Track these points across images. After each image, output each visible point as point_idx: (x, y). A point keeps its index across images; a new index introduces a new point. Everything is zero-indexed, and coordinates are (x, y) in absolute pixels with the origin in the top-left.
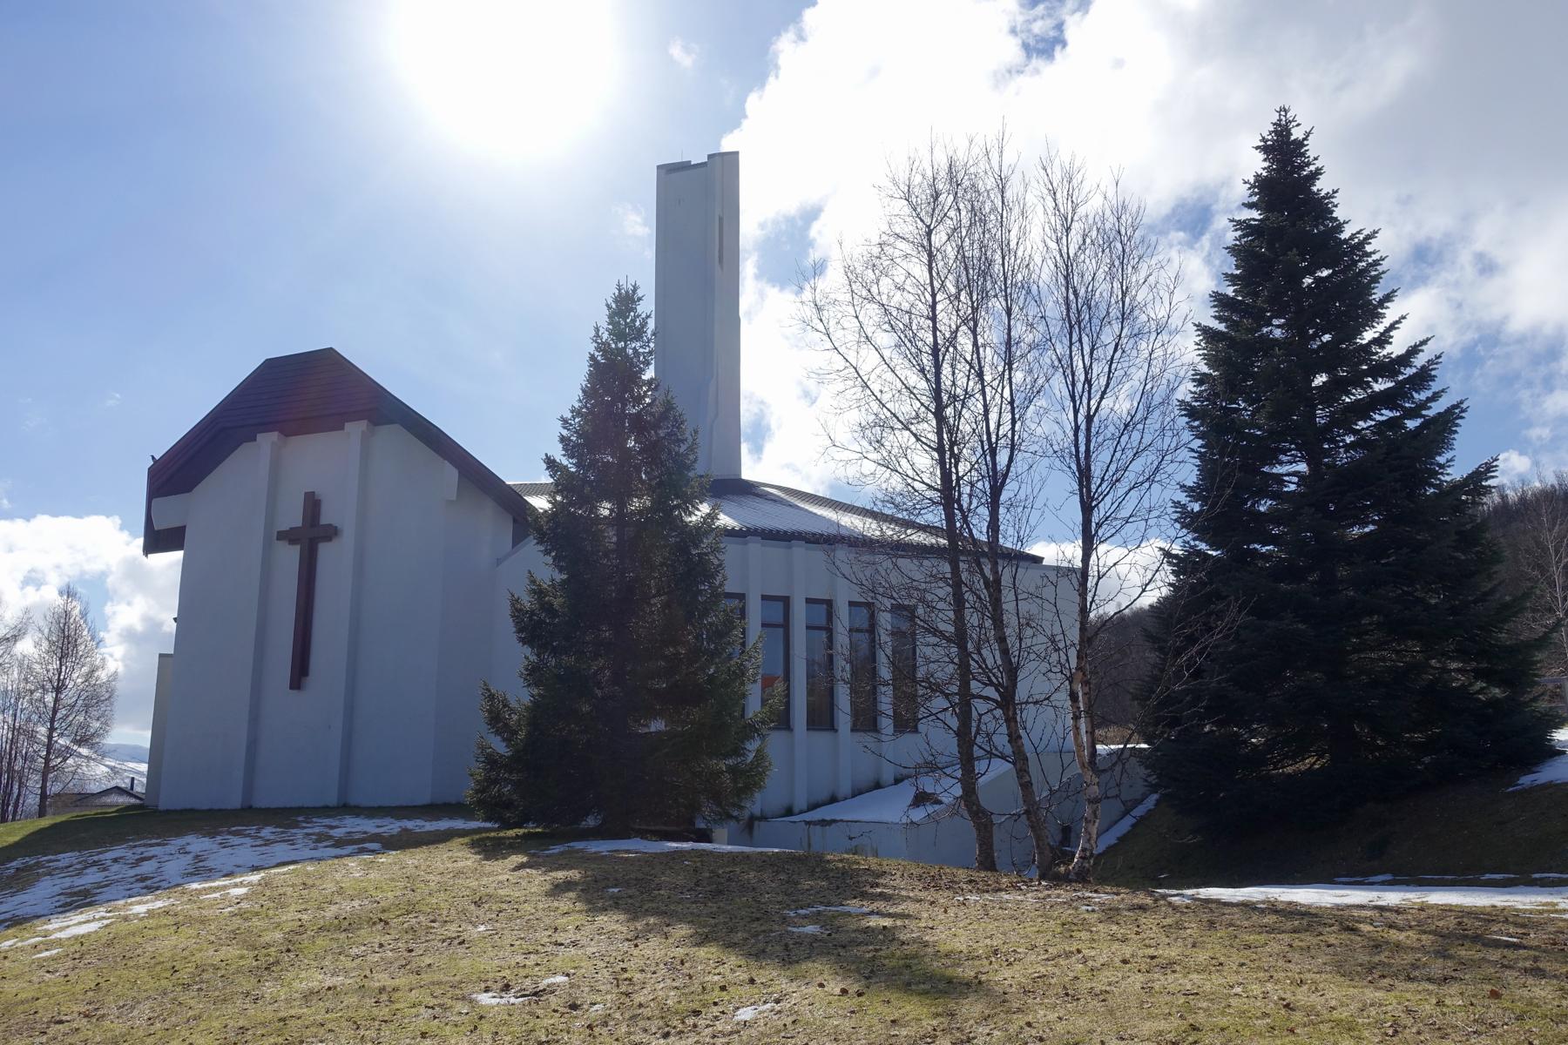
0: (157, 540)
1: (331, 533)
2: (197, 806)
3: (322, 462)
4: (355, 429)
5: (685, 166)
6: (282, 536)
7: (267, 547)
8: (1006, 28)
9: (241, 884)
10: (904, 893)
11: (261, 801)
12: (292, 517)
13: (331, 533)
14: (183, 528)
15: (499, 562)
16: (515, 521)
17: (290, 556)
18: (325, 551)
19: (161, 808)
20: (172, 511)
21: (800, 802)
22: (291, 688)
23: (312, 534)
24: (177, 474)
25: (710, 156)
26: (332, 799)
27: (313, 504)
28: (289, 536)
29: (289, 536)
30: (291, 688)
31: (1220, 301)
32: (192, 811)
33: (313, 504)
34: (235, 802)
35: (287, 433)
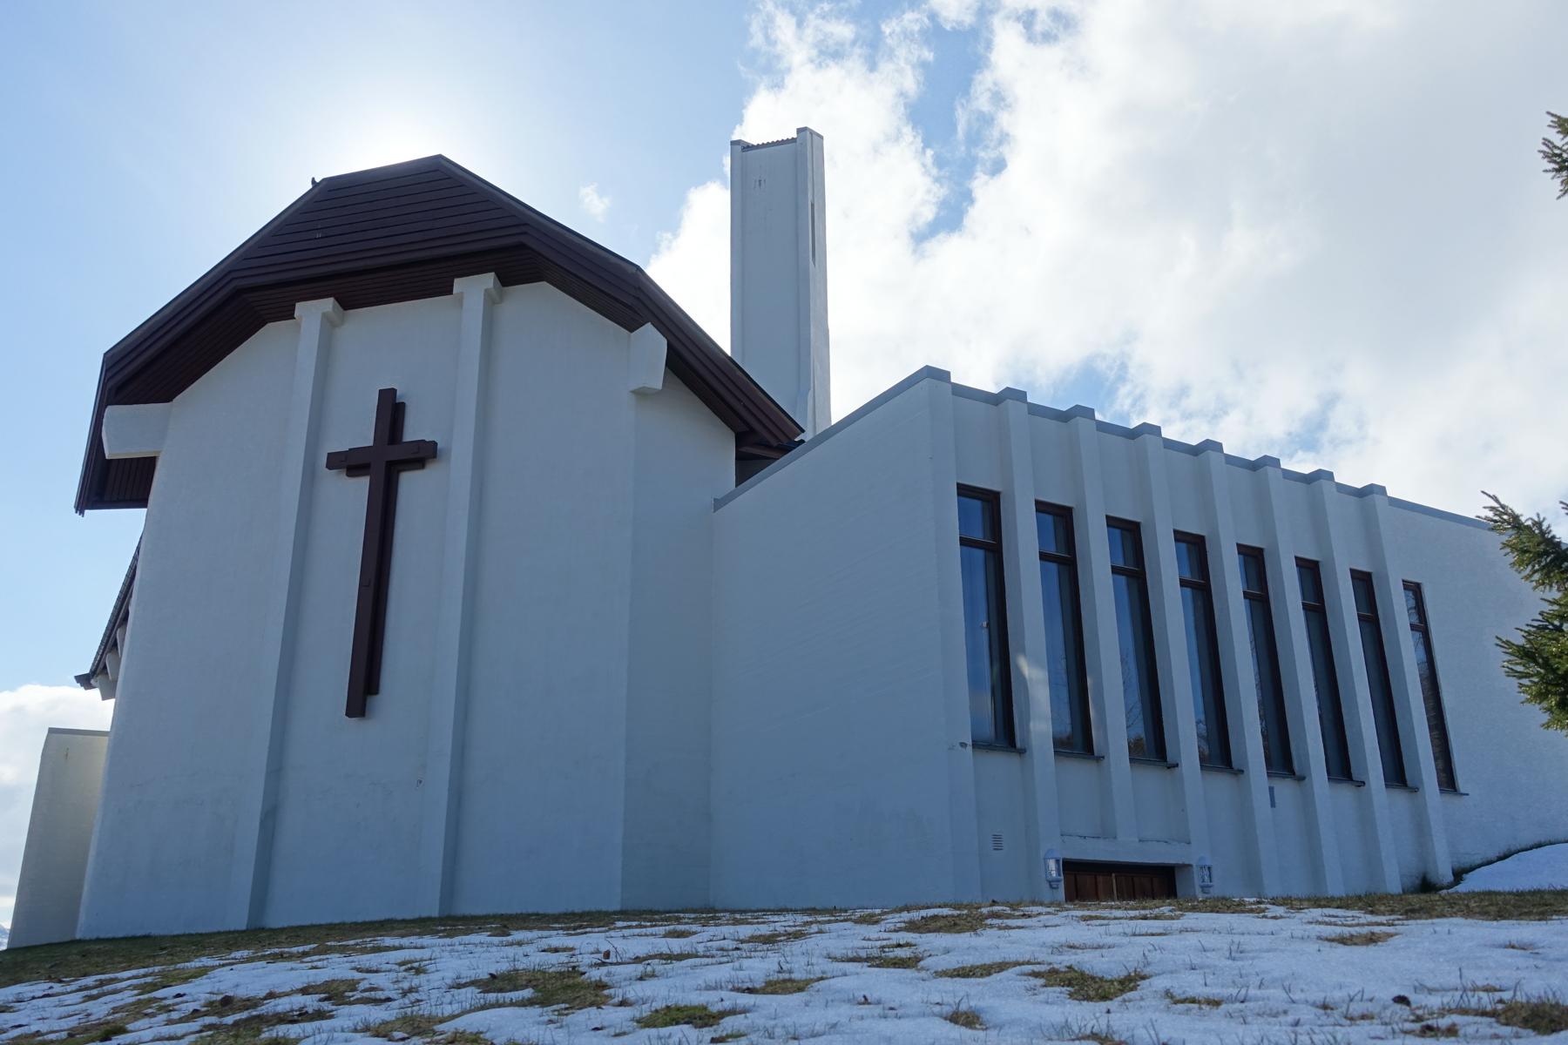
0: (111, 481)
1: (424, 455)
2: (155, 932)
3: (425, 348)
4: (474, 289)
7: (309, 479)
10: (985, 911)
12: (359, 432)
15: (719, 504)
18: (409, 482)
20: (133, 430)
21: (1444, 873)
22: (349, 713)
23: (389, 456)
24: (158, 363)
27: (391, 410)
28: (349, 463)
29: (349, 463)
30: (349, 713)
31: (937, 180)
33: (391, 410)
35: (507, 279)
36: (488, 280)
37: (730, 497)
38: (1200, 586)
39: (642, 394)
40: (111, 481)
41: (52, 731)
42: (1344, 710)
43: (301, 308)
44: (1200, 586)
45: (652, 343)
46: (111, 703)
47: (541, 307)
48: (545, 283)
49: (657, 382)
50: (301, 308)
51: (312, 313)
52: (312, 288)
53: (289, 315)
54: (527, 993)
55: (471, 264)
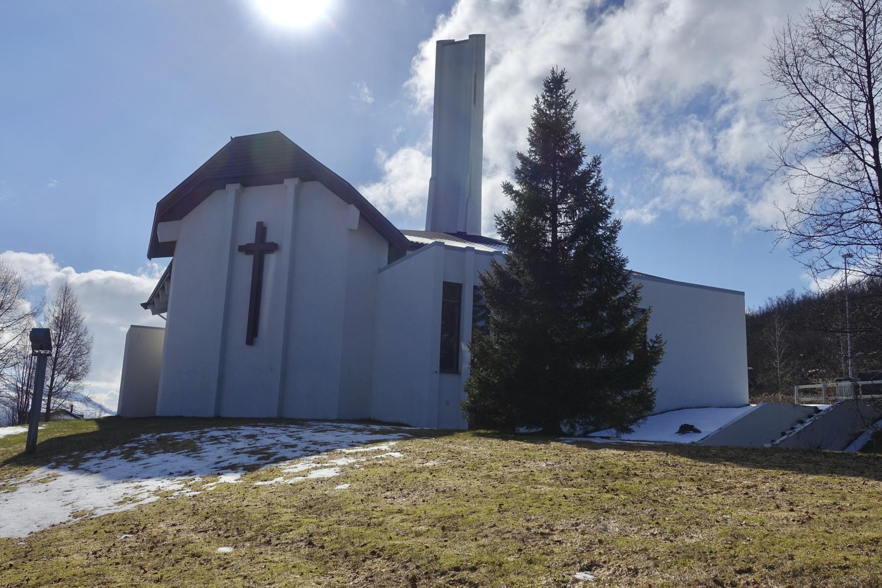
0: (157, 249)
1: (274, 248)
3: (272, 206)
4: (291, 184)
5: (451, 43)
6: (242, 249)
8: (513, 23)
9: (289, 476)
11: (225, 414)
12: (249, 237)
13: (274, 248)
14: (518, 154)
15: (380, 271)
16: (390, 245)
17: (246, 262)
18: (271, 261)
19: (157, 414)
23: (261, 248)
24: (173, 208)
25: (470, 36)
26: (274, 414)
27: (261, 229)
28: (245, 249)
29: (245, 249)
32: (181, 417)
33: (261, 229)
34: (211, 413)
36: (237, 186)
37: (385, 269)
40: (157, 249)
41: (132, 326)
43: (228, 186)
48: (217, 191)
49: (356, 227)
50: (228, 186)
53: (282, 182)
54: (53, 464)
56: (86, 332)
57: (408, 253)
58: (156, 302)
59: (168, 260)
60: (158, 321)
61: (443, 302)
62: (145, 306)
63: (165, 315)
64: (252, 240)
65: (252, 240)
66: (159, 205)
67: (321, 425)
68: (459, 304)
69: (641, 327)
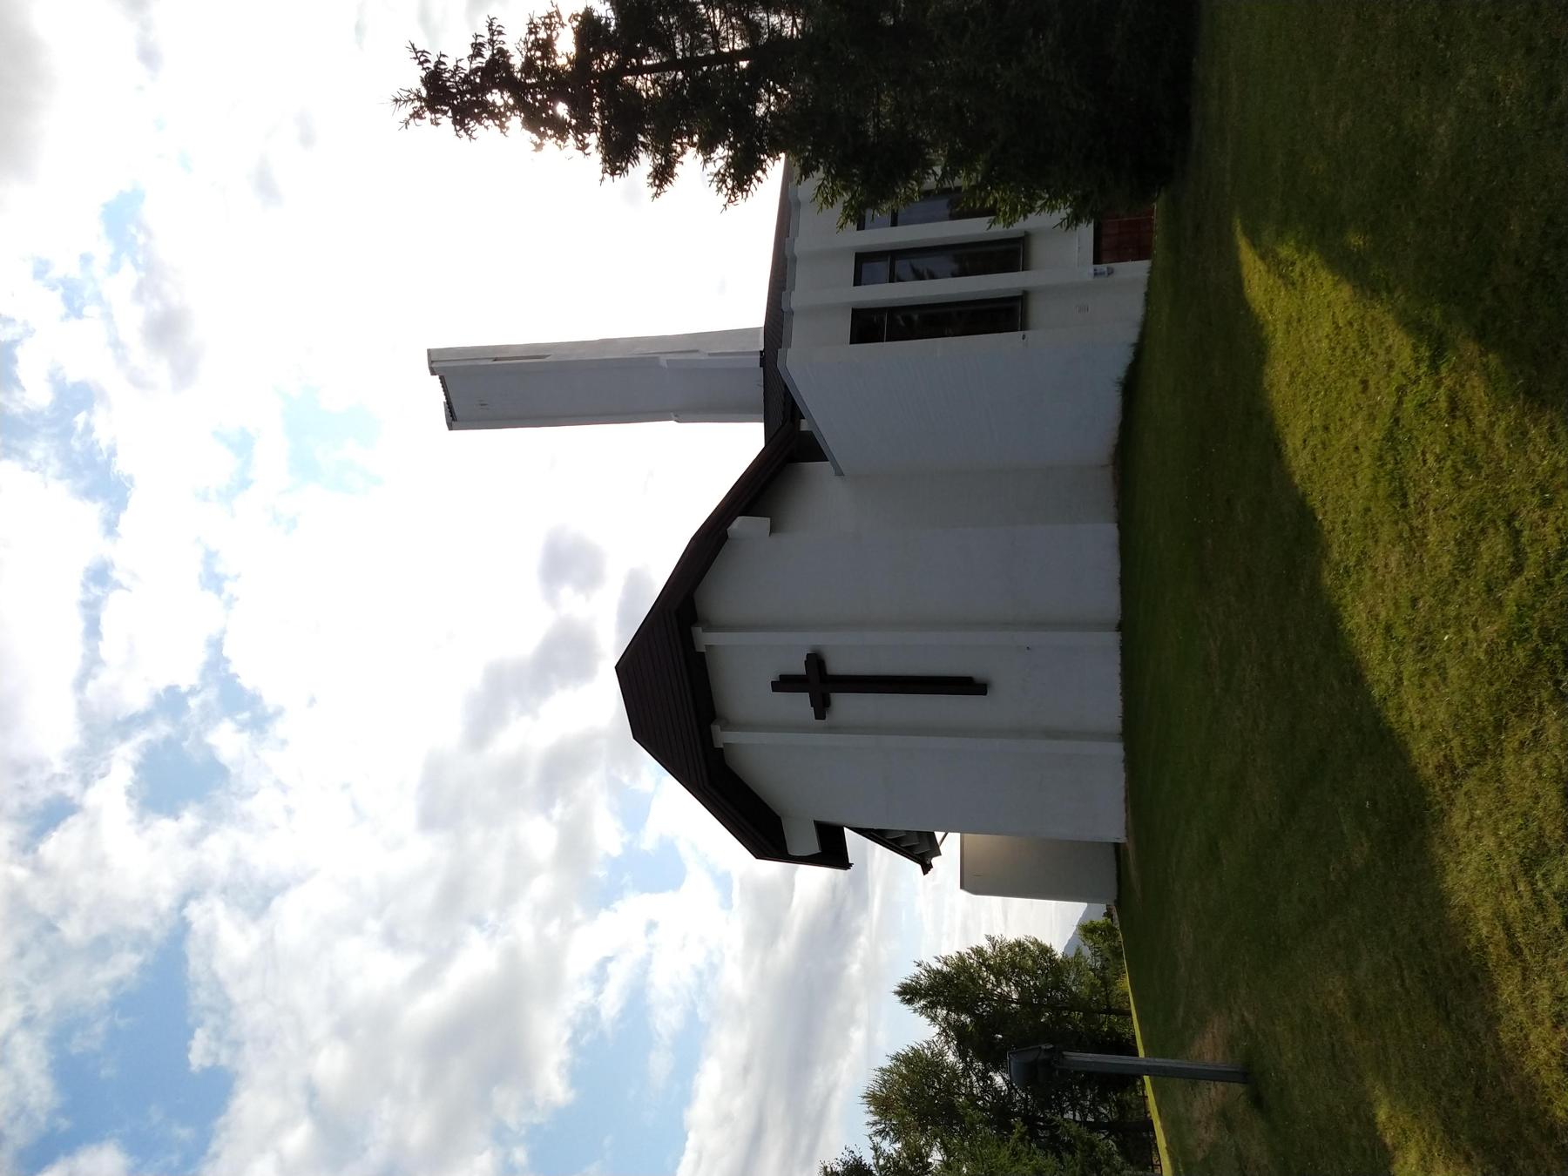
1: (816, 661)
3: (747, 664)
4: (705, 639)
6: (820, 714)
7: (832, 729)
12: (799, 704)
13: (816, 661)
15: (839, 473)
17: (845, 705)
18: (837, 665)
23: (818, 682)
24: (761, 830)
27: (785, 683)
28: (821, 707)
29: (821, 707)
33: (785, 683)
38: (974, 258)
39: (773, 530)
40: (832, 854)
42: (1113, 568)
44: (974, 258)
45: (740, 525)
46: (1135, 272)
47: (726, 595)
49: (765, 522)
51: (724, 737)
52: (707, 739)
55: (688, 641)
56: (979, 952)
57: (804, 426)
58: (921, 850)
59: (849, 835)
60: (950, 845)
61: (890, 339)
62: (926, 868)
63: (939, 835)
64: (805, 698)
65: (805, 698)
66: (758, 856)
67: (922, 264)
68: (892, 311)
69: (890, 1071)
